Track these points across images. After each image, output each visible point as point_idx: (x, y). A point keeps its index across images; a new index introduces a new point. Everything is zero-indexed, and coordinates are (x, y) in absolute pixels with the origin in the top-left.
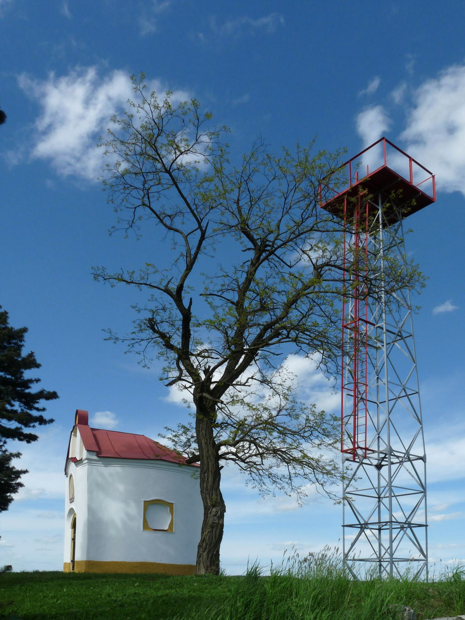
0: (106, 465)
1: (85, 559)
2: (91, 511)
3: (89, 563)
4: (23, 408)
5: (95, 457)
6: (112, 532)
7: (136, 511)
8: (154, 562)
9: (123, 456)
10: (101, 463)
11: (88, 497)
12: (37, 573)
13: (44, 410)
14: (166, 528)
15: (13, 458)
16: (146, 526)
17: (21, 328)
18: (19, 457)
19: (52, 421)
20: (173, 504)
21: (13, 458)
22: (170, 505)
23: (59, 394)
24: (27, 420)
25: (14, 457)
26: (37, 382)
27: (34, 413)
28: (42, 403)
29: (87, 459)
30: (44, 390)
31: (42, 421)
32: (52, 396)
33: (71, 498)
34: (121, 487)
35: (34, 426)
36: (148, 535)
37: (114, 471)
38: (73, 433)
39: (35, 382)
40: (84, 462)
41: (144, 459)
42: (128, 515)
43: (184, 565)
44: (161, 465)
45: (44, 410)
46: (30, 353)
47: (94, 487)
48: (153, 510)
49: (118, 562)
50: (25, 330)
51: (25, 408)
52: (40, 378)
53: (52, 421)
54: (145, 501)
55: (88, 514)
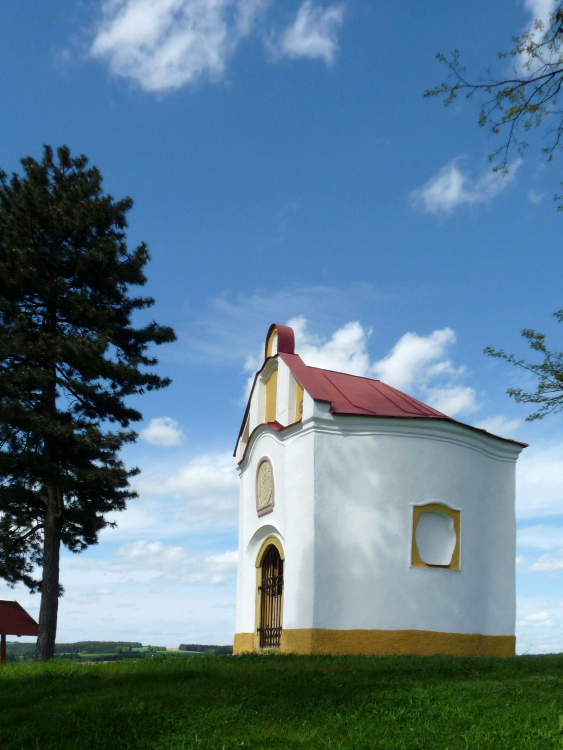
0: (346, 432)
1: (308, 624)
2: (323, 530)
3: (319, 635)
4: (122, 358)
5: (327, 416)
6: (356, 570)
7: (399, 525)
8: (427, 630)
9: (379, 412)
10: (337, 428)
11: (316, 498)
12: (119, 642)
13: (154, 362)
14: (447, 561)
15: (124, 442)
16: (416, 559)
17: (123, 200)
18: (134, 441)
19: (167, 382)
20: (458, 512)
21: (124, 442)
22: (455, 514)
23: (177, 332)
24: (130, 380)
25: (126, 442)
26: (149, 306)
27: (143, 369)
28: (151, 350)
29: (314, 419)
30: (155, 324)
31: (155, 382)
32: (165, 335)
33: (263, 504)
34: (374, 478)
35: (141, 391)
36: (420, 575)
37: (363, 445)
38: (260, 377)
39: (145, 305)
40: (305, 427)
41: (415, 418)
42: (387, 536)
43: (473, 636)
44: (444, 431)
45: (154, 362)
46: (140, 245)
47: (328, 478)
48: (430, 523)
49: (367, 632)
50: (127, 204)
51: (125, 358)
52: (154, 297)
53: (167, 382)
54: (415, 507)
55: (315, 535)
